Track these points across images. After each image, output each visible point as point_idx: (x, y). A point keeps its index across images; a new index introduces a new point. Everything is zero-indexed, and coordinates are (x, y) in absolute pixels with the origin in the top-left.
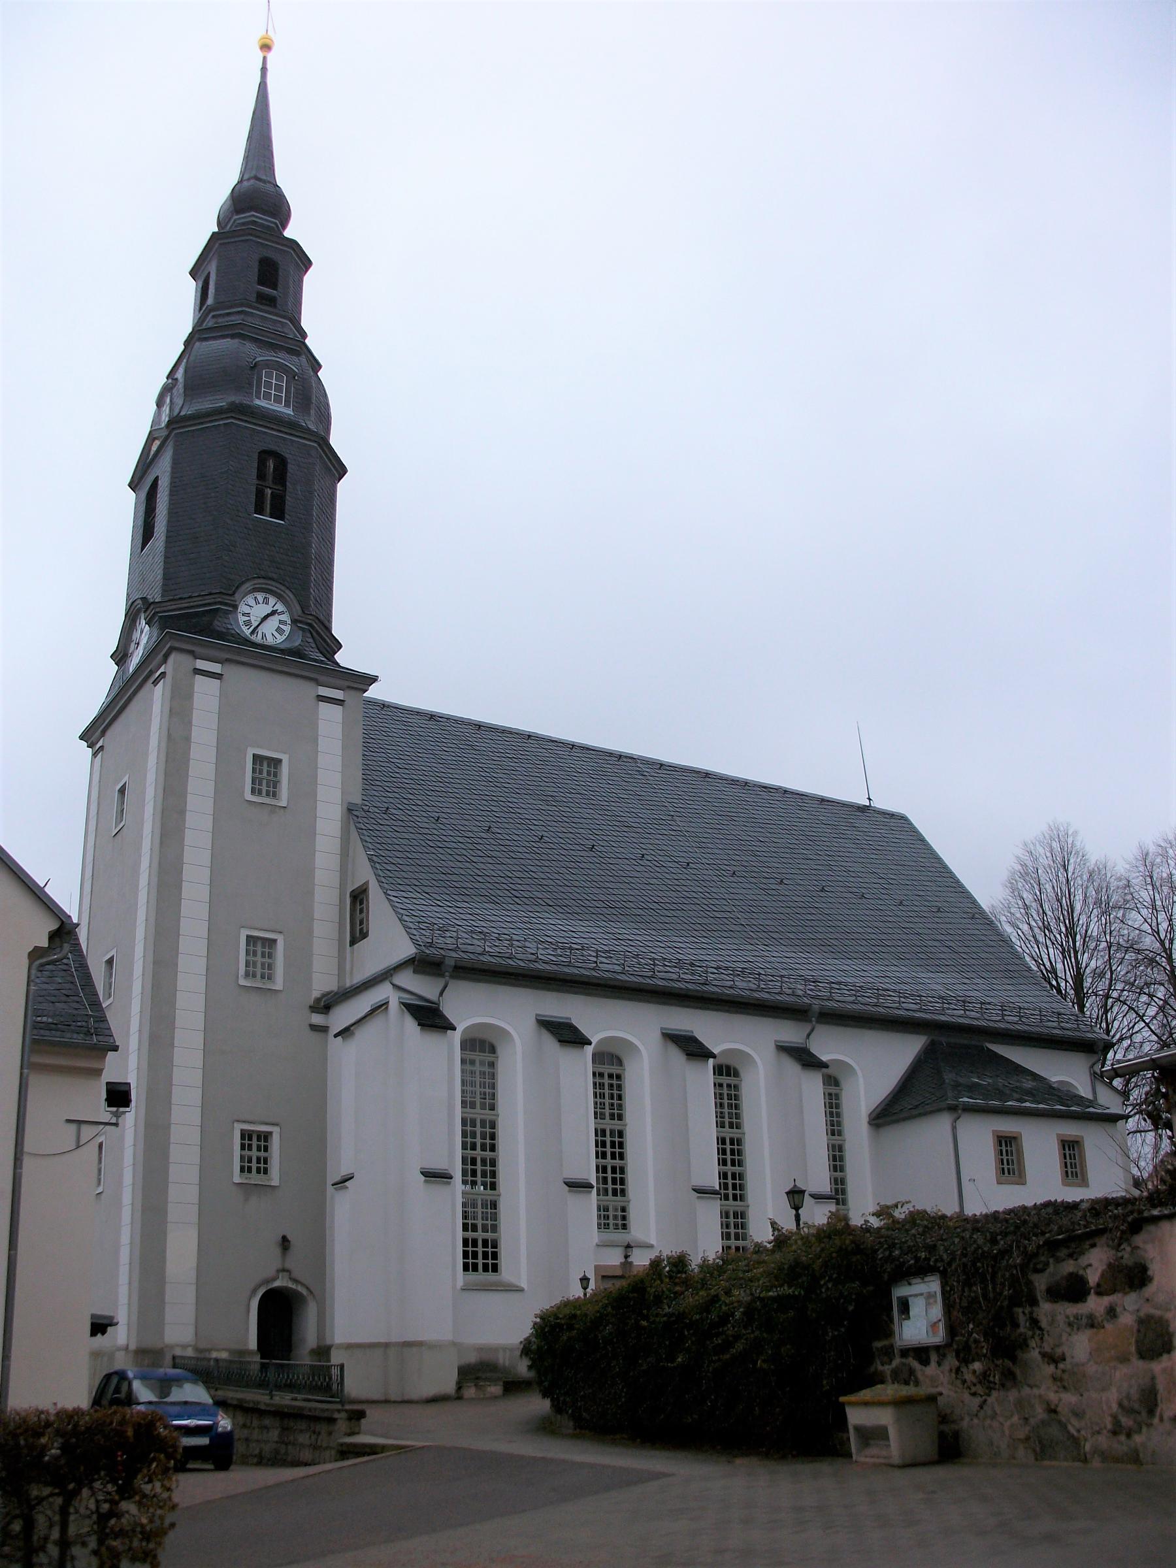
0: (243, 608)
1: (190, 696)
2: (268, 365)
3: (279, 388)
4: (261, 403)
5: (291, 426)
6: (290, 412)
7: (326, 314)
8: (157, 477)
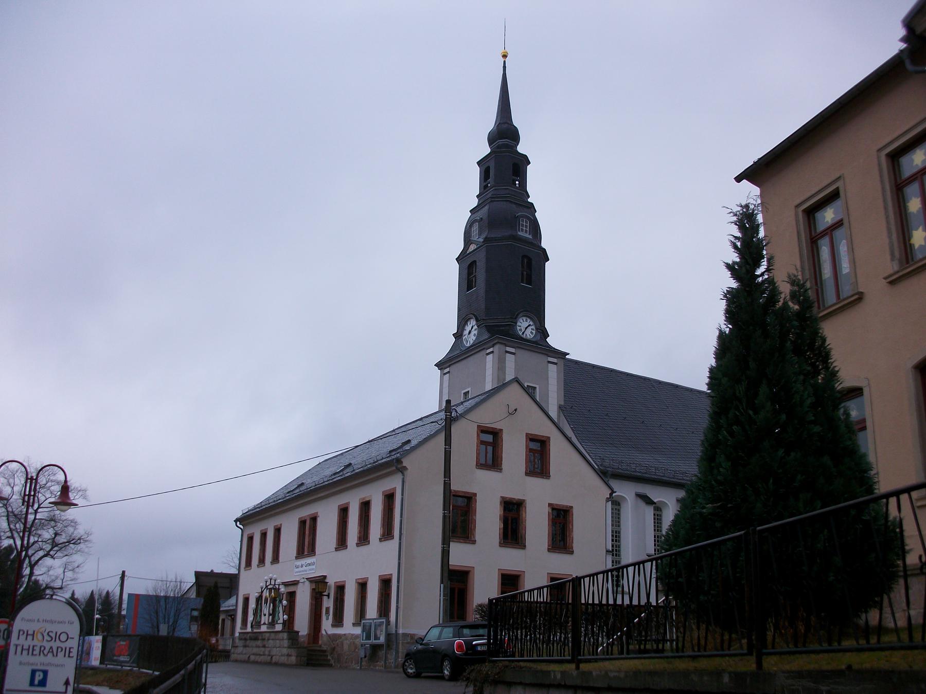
0: (519, 324)
1: (504, 362)
2: (523, 216)
3: (526, 227)
4: (520, 233)
5: (532, 243)
6: (530, 237)
7: (539, 187)
8: (475, 261)
